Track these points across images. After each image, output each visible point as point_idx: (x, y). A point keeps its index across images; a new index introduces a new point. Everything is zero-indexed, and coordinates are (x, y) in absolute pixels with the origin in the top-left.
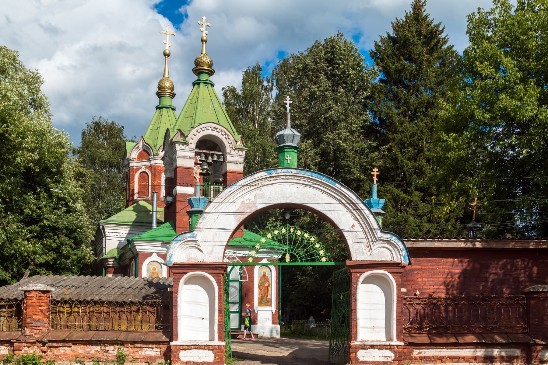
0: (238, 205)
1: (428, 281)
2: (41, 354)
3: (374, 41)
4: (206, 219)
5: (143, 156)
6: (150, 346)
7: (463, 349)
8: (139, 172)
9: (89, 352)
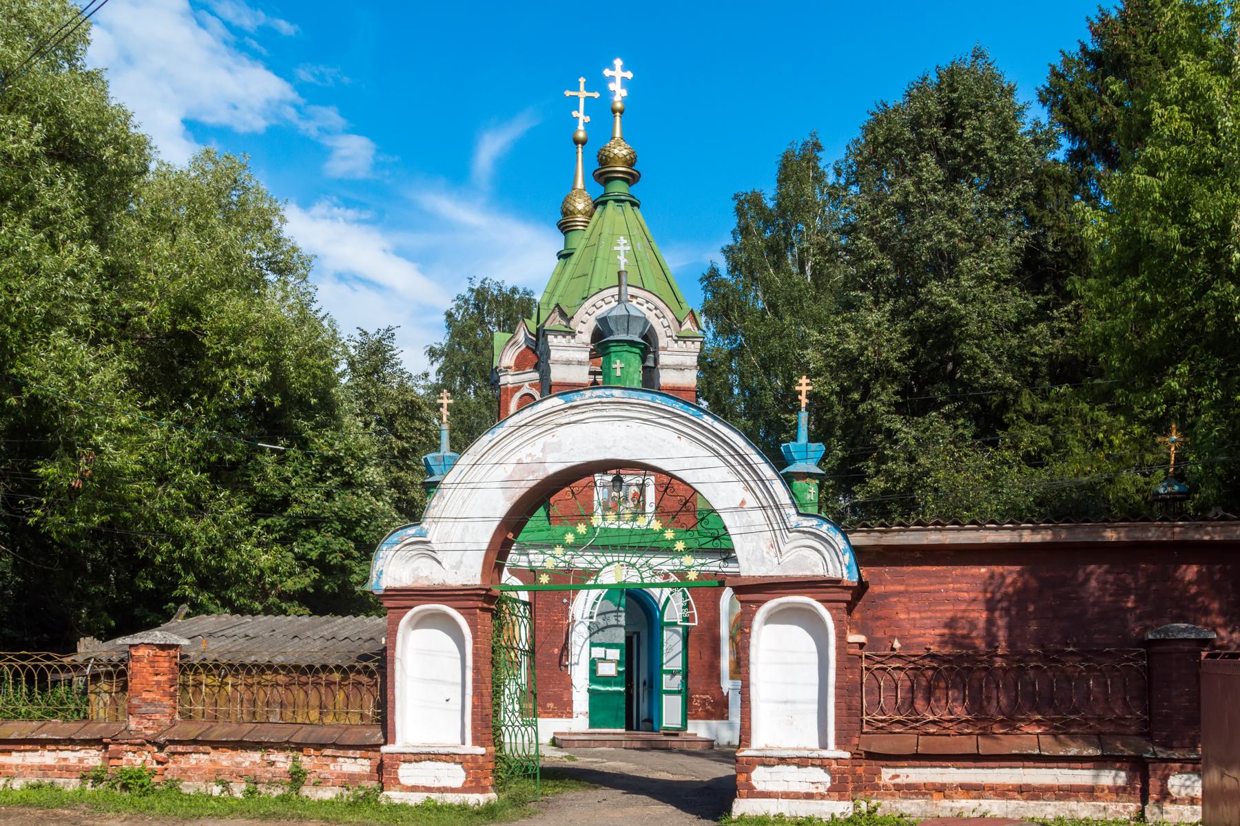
0: (510, 468)
1: (922, 618)
2: (155, 766)
3: (1050, 65)
4: (446, 499)
5: (526, 360)
6: (350, 753)
7: (993, 768)
8: (518, 395)
9: (241, 763)
